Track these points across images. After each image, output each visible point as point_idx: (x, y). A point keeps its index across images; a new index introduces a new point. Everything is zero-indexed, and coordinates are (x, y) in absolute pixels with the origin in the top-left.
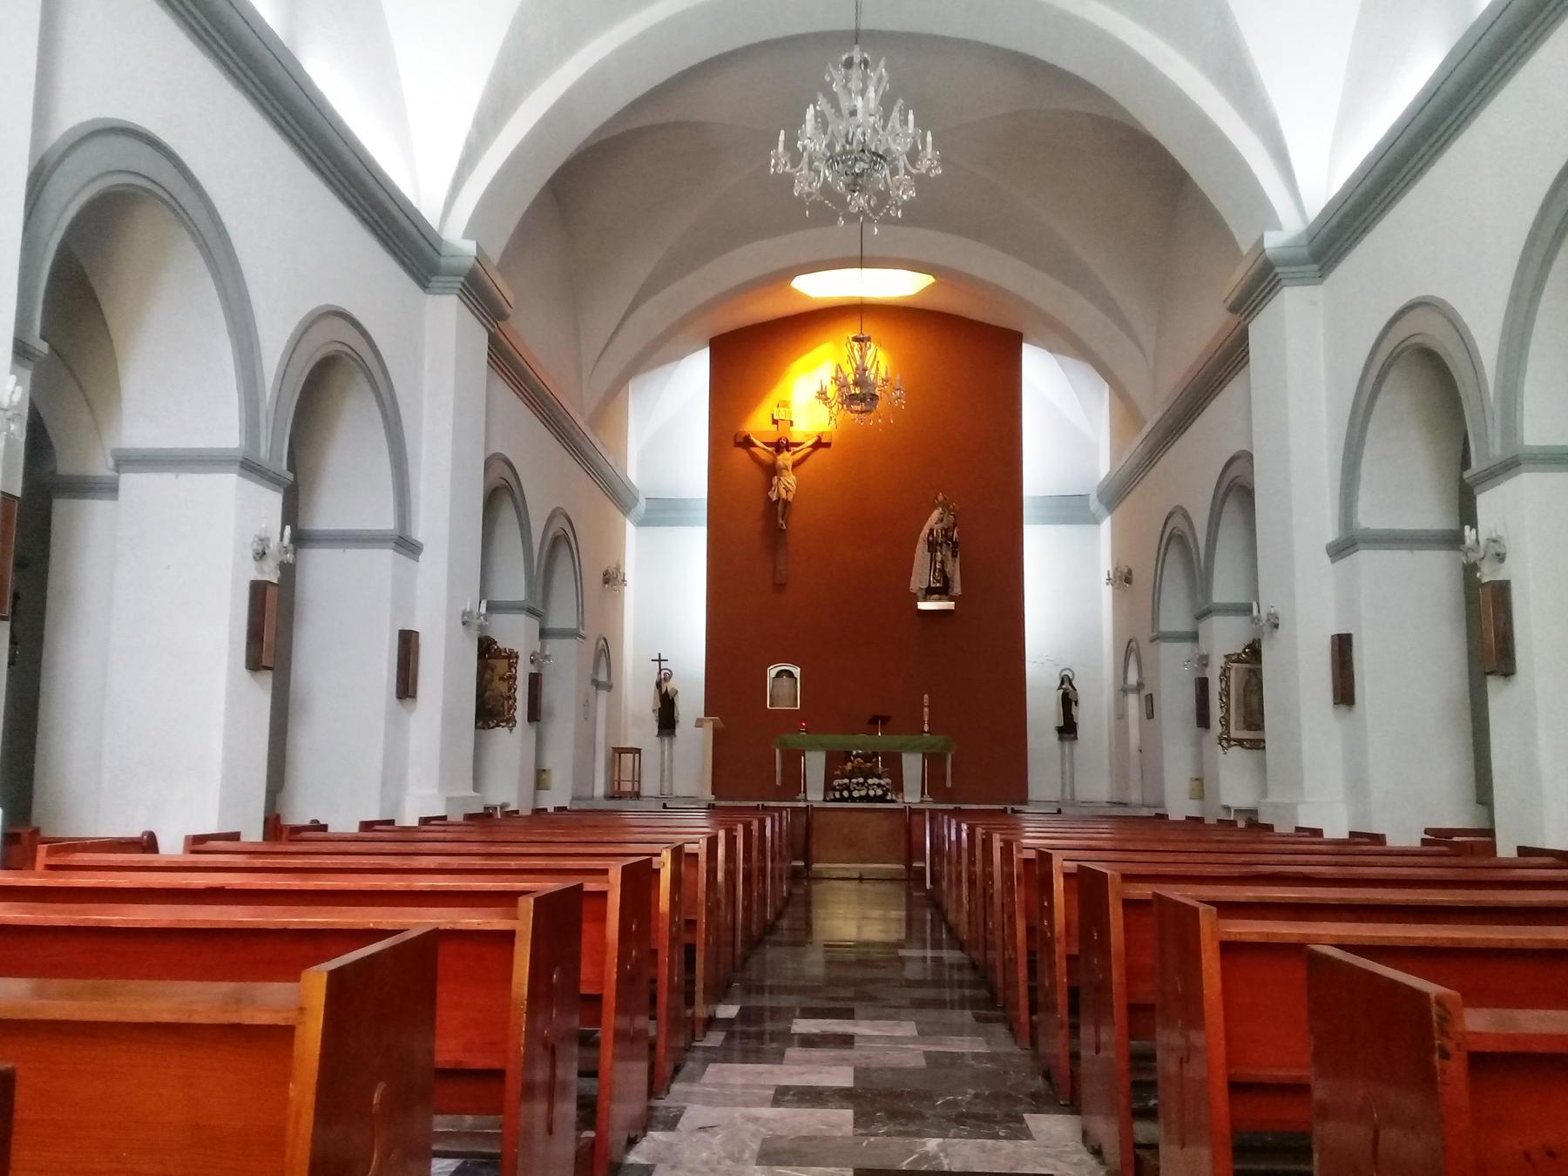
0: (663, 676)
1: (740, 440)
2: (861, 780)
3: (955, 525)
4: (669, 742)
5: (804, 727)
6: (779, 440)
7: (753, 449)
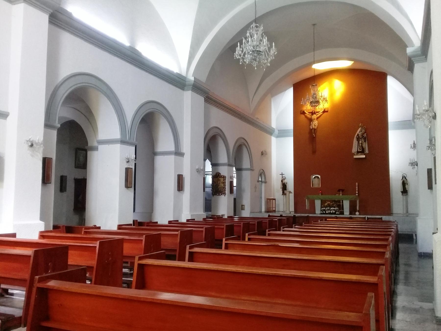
0: (283, 179)
1: (302, 112)
2: (329, 208)
3: (365, 132)
4: (285, 197)
5: (320, 192)
6: (313, 111)
7: (306, 114)
